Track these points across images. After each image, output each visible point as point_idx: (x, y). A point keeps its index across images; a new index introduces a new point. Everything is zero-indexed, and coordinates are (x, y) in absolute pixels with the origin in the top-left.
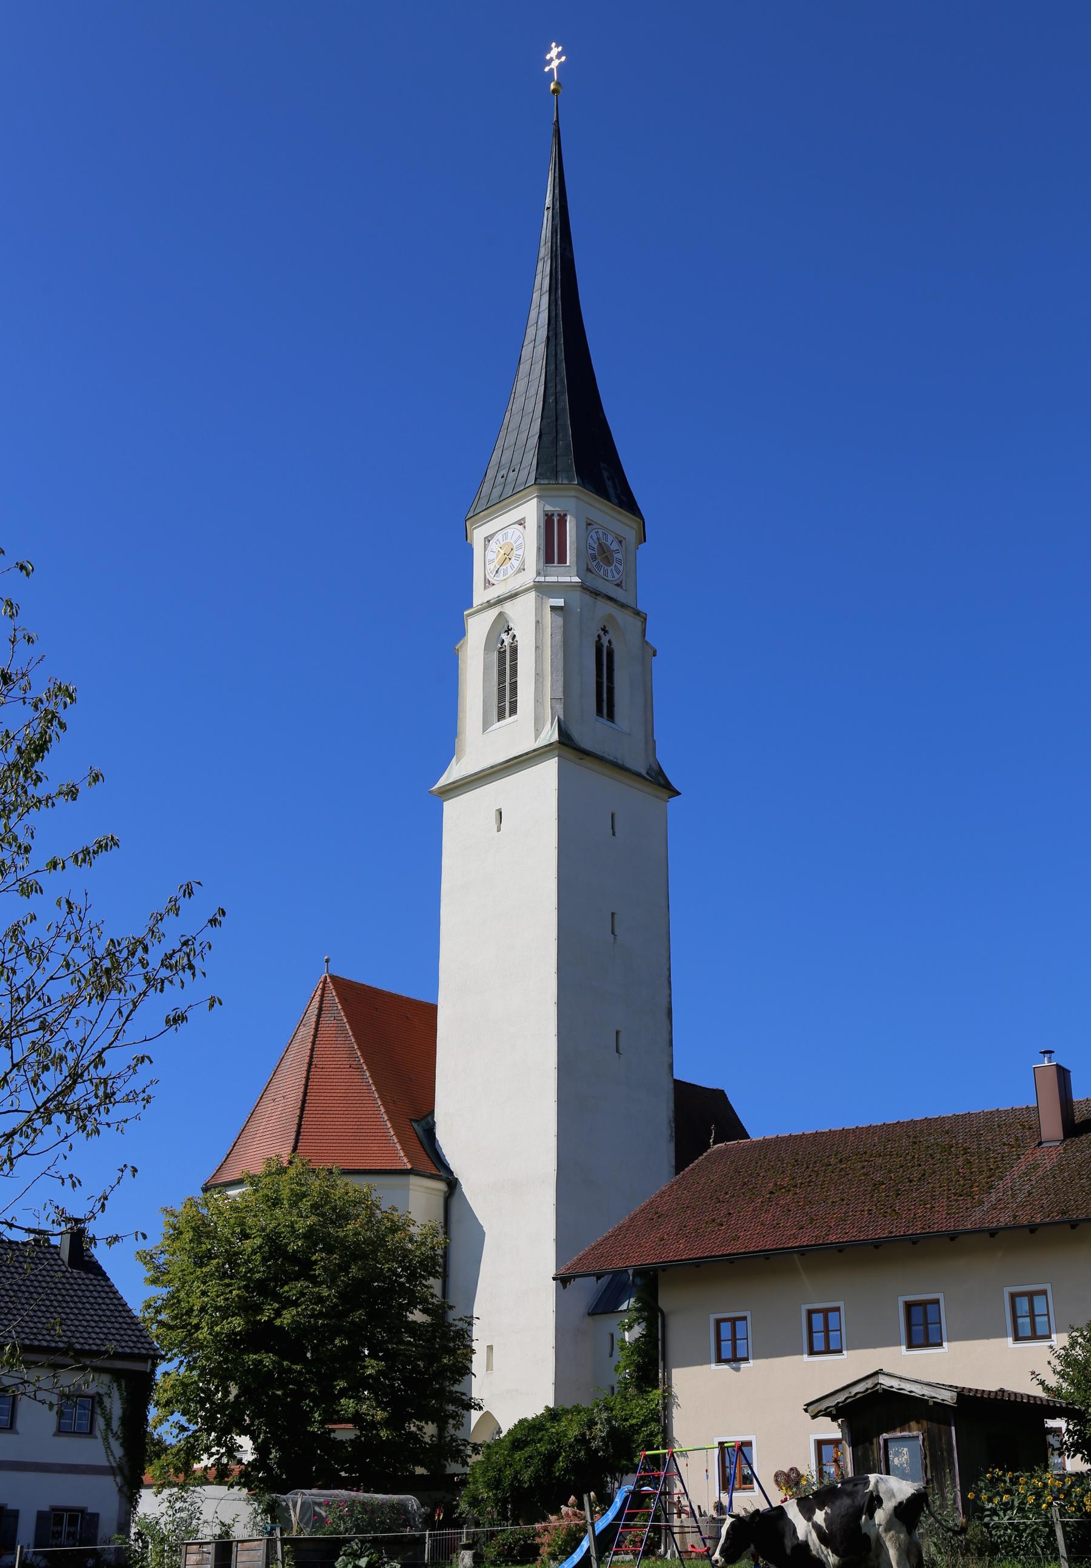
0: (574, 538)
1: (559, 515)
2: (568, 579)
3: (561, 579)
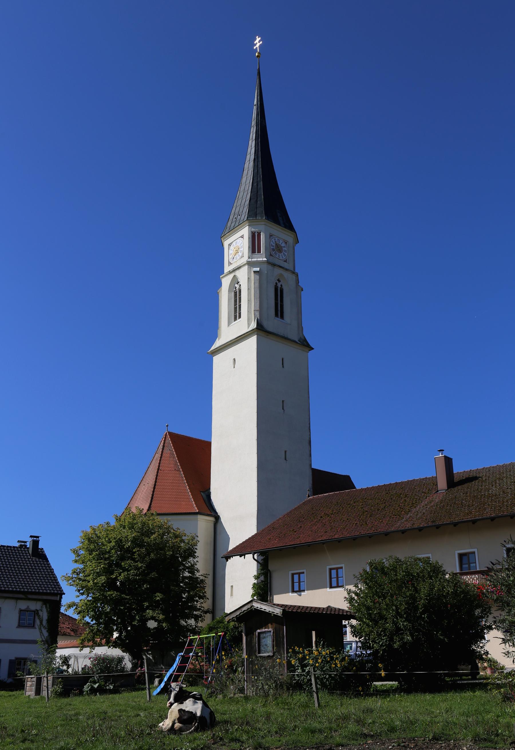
1: (258, 232)
2: (261, 259)
3: (258, 259)
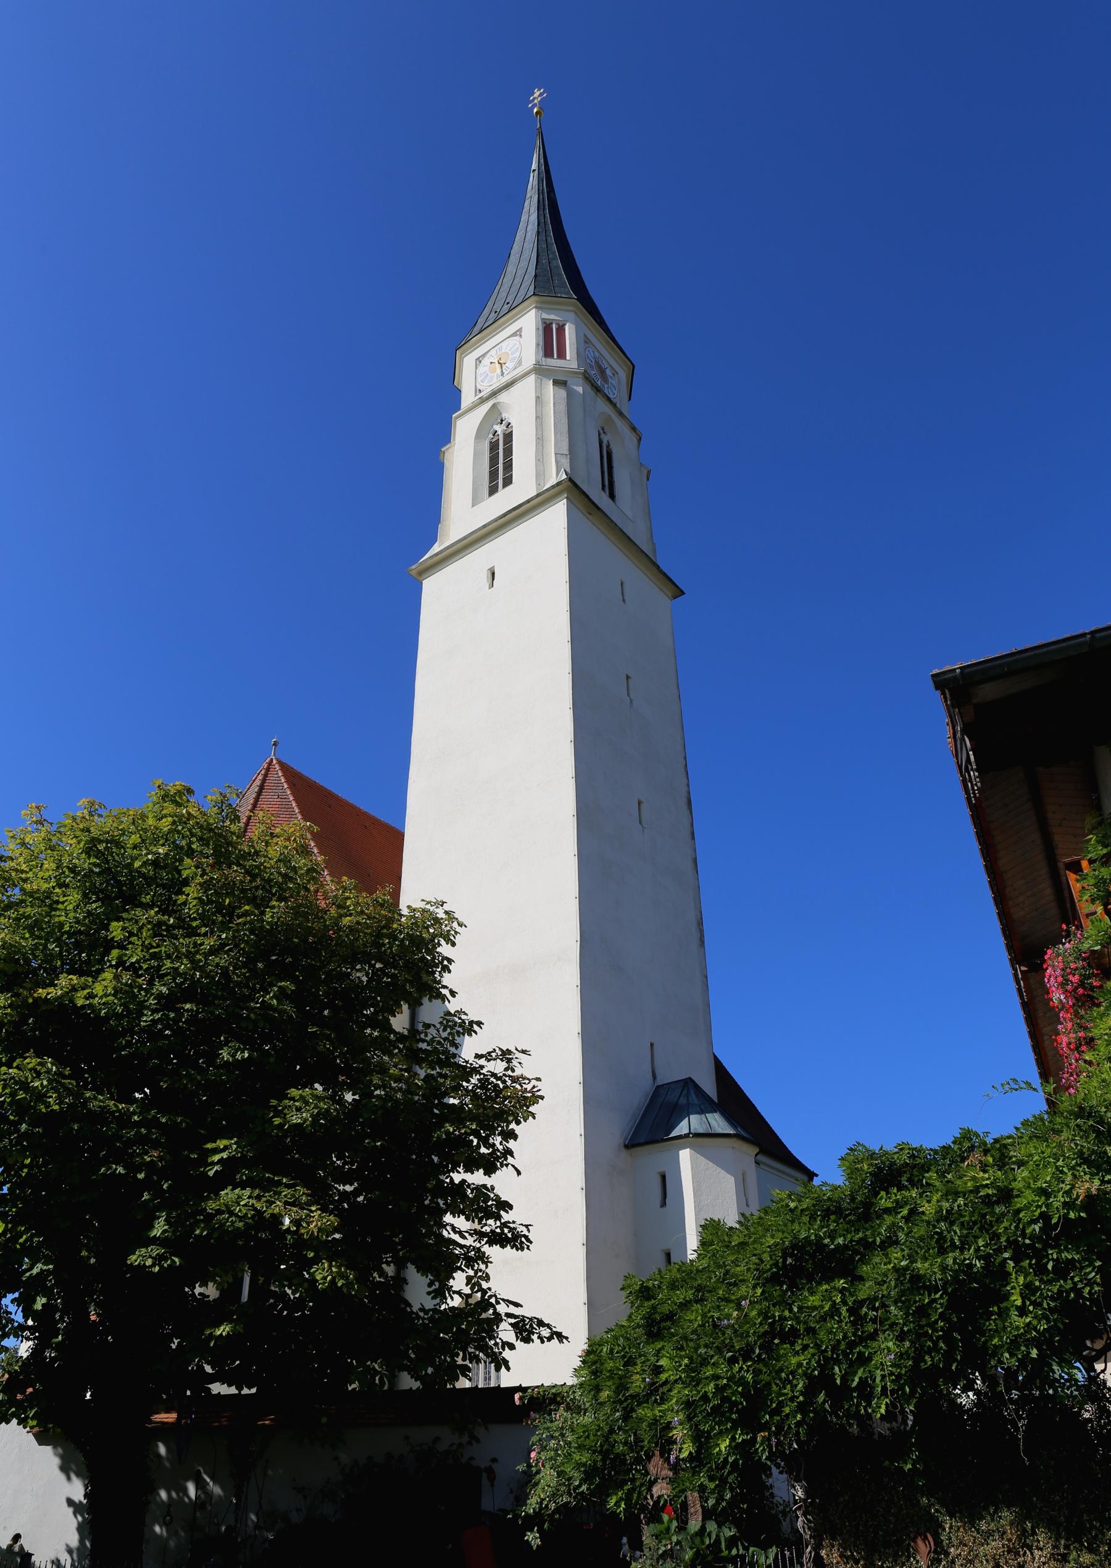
0: (574, 341)
1: (558, 324)
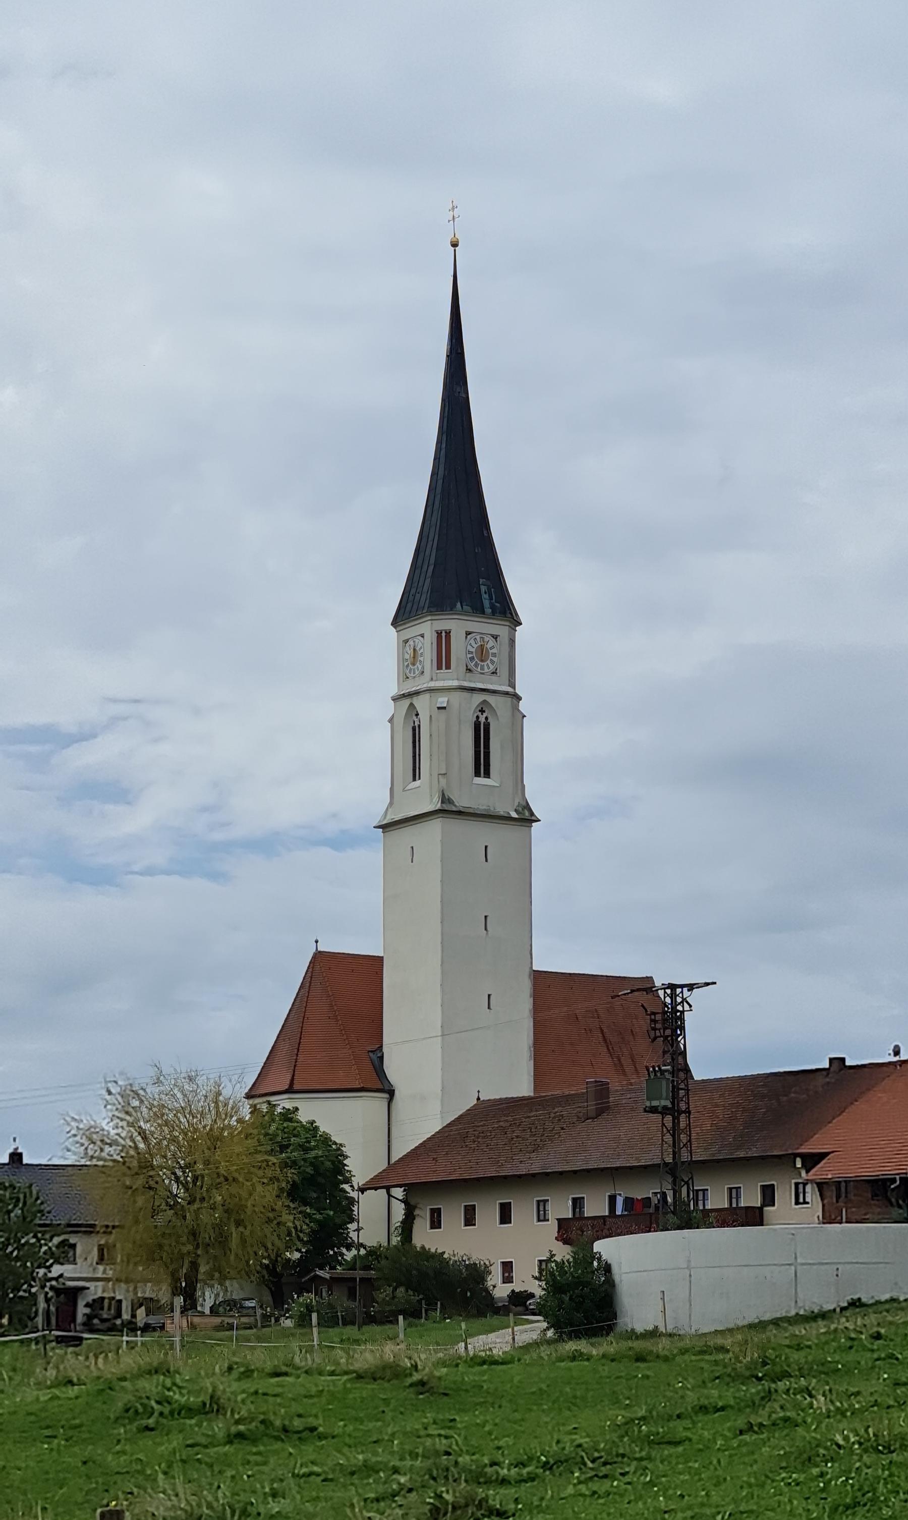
1: (446, 632)
